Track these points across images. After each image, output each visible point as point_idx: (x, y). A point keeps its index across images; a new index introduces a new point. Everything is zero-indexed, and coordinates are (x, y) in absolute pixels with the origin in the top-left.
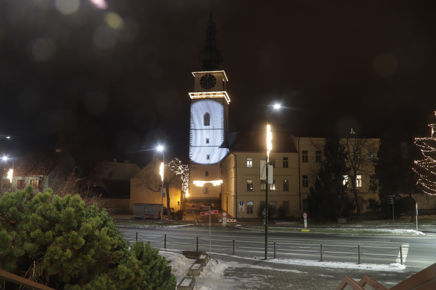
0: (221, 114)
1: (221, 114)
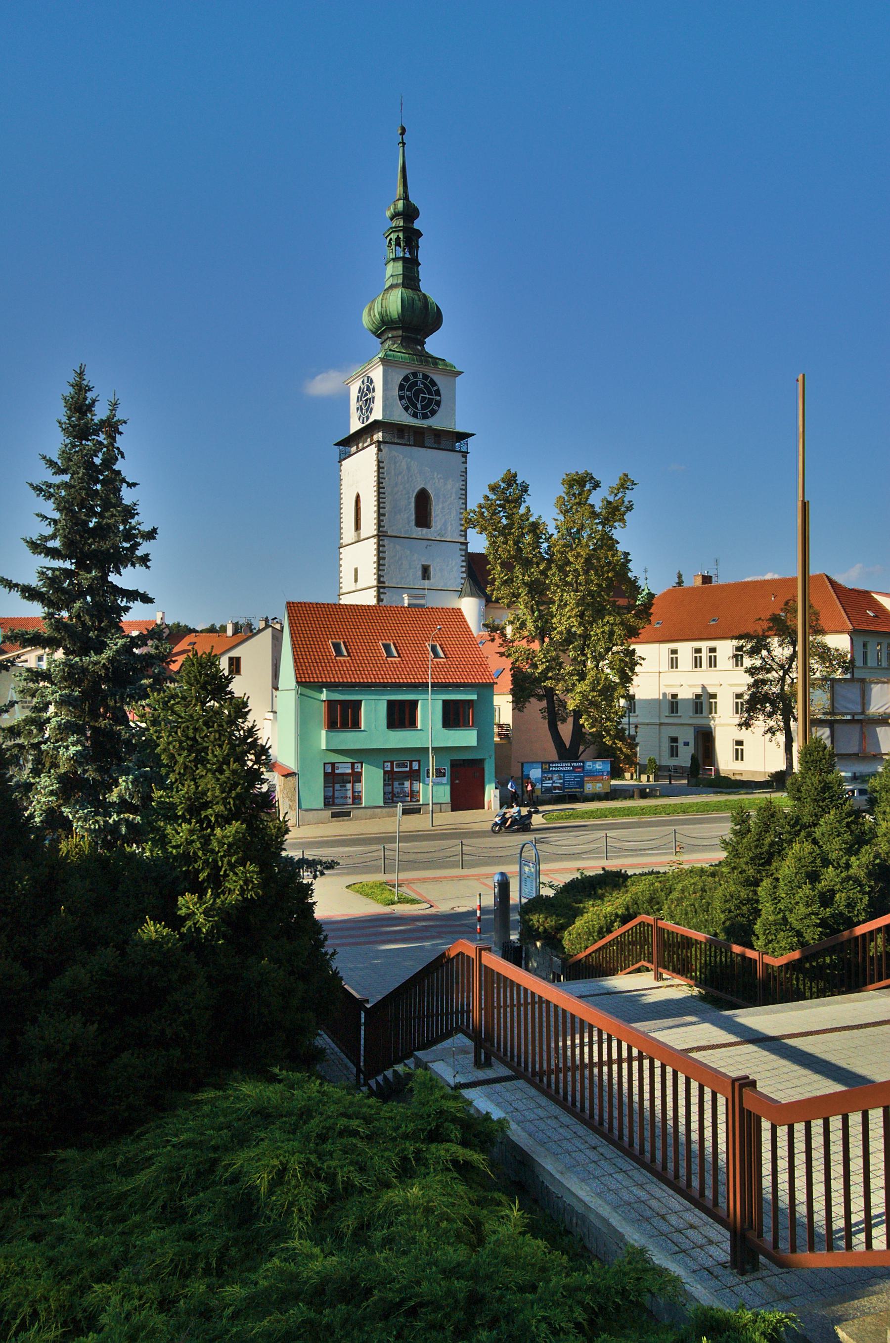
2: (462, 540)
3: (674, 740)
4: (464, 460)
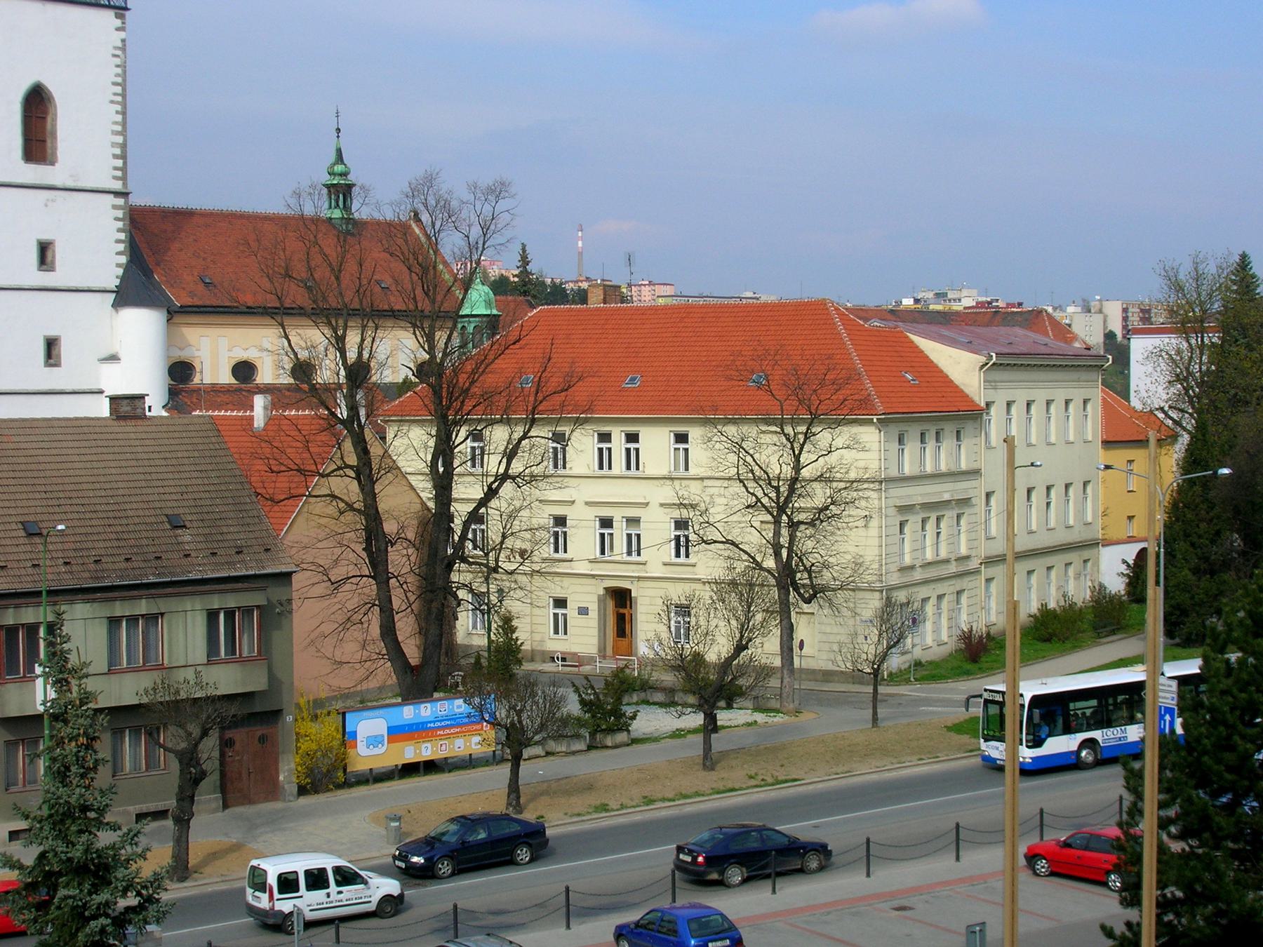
0: (112, 102)
1: (112, 102)
2: (118, 186)
3: (561, 603)
4: (118, 23)
